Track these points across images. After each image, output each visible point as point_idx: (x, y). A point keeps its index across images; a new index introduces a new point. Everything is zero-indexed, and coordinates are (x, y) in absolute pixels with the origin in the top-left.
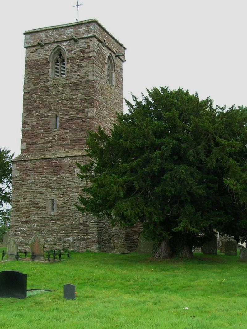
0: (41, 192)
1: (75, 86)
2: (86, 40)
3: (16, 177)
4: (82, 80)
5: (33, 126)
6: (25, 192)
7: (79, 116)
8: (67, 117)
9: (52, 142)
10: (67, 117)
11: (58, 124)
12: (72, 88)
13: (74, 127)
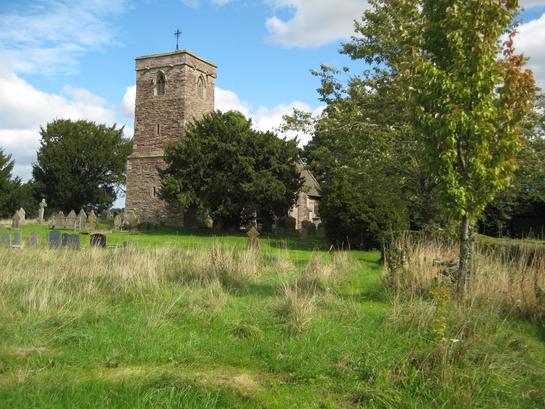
0: (146, 182)
1: (171, 102)
2: (179, 67)
3: (129, 170)
4: (176, 98)
5: (142, 132)
6: (135, 181)
7: (174, 125)
8: (165, 126)
9: (155, 144)
10: (165, 126)
11: (160, 131)
12: (170, 104)
13: (170, 134)
